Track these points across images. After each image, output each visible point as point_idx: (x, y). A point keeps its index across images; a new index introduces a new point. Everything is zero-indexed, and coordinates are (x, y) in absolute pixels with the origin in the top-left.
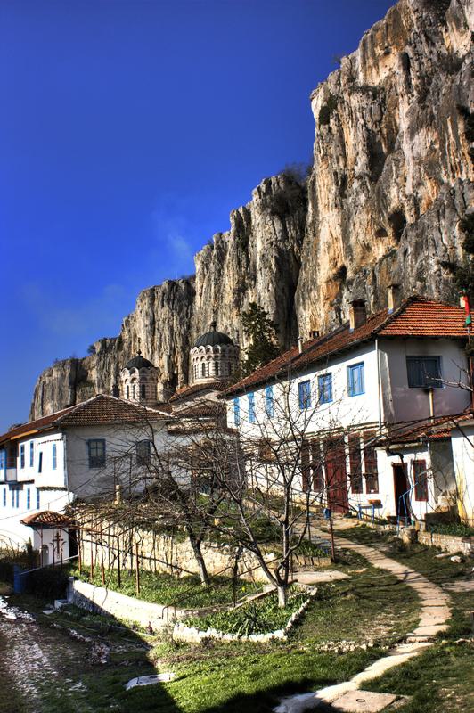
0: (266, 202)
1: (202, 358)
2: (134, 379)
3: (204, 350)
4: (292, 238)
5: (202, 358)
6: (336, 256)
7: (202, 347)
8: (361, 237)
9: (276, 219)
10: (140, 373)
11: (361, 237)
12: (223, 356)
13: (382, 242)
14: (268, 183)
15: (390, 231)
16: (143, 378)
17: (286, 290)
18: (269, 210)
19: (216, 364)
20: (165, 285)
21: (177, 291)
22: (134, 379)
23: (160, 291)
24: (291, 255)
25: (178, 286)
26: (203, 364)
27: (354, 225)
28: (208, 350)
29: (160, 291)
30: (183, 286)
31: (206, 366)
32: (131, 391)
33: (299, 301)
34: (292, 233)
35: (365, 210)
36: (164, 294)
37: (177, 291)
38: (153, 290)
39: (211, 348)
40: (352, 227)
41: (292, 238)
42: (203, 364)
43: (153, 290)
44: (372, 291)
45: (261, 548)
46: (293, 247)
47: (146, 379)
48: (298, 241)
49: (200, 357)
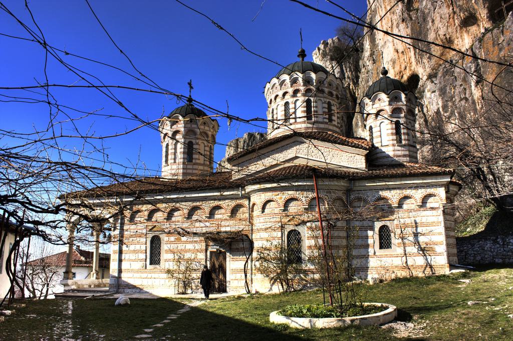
0: (326, 52)
1: (285, 94)
2: (176, 133)
3: (288, 82)
4: (348, 77)
5: (285, 94)
6: (402, 69)
7: (285, 77)
8: (441, 32)
9: (334, 63)
10: (186, 123)
11: (441, 32)
12: (319, 90)
13: (467, 32)
14: (326, 44)
15: (483, 13)
16: (189, 132)
17: (345, 119)
18: (329, 57)
19: (308, 102)
20: (246, 136)
21: (254, 140)
22: (176, 133)
23: (242, 141)
24: (348, 91)
25: (255, 137)
26: (287, 104)
27: (433, 21)
28: (294, 81)
29: (242, 141)
30: (258, 137)
31: (291, 106)
32: (171, 151)
33: (357, 125)
34: (348, 74)
35: (445, 5)
36: (245, 142)
37: (254, 140)
38: (237, 140)
39: (300, 76)
40: (430, 24)
41: (348, 77)
42: (287, 104)
43: (237, 140)
44: (473, 69)
45: (278, 255)
46: (349, 84)
47: (195, 134)
48: (353, 80)
49: (280, 93)
